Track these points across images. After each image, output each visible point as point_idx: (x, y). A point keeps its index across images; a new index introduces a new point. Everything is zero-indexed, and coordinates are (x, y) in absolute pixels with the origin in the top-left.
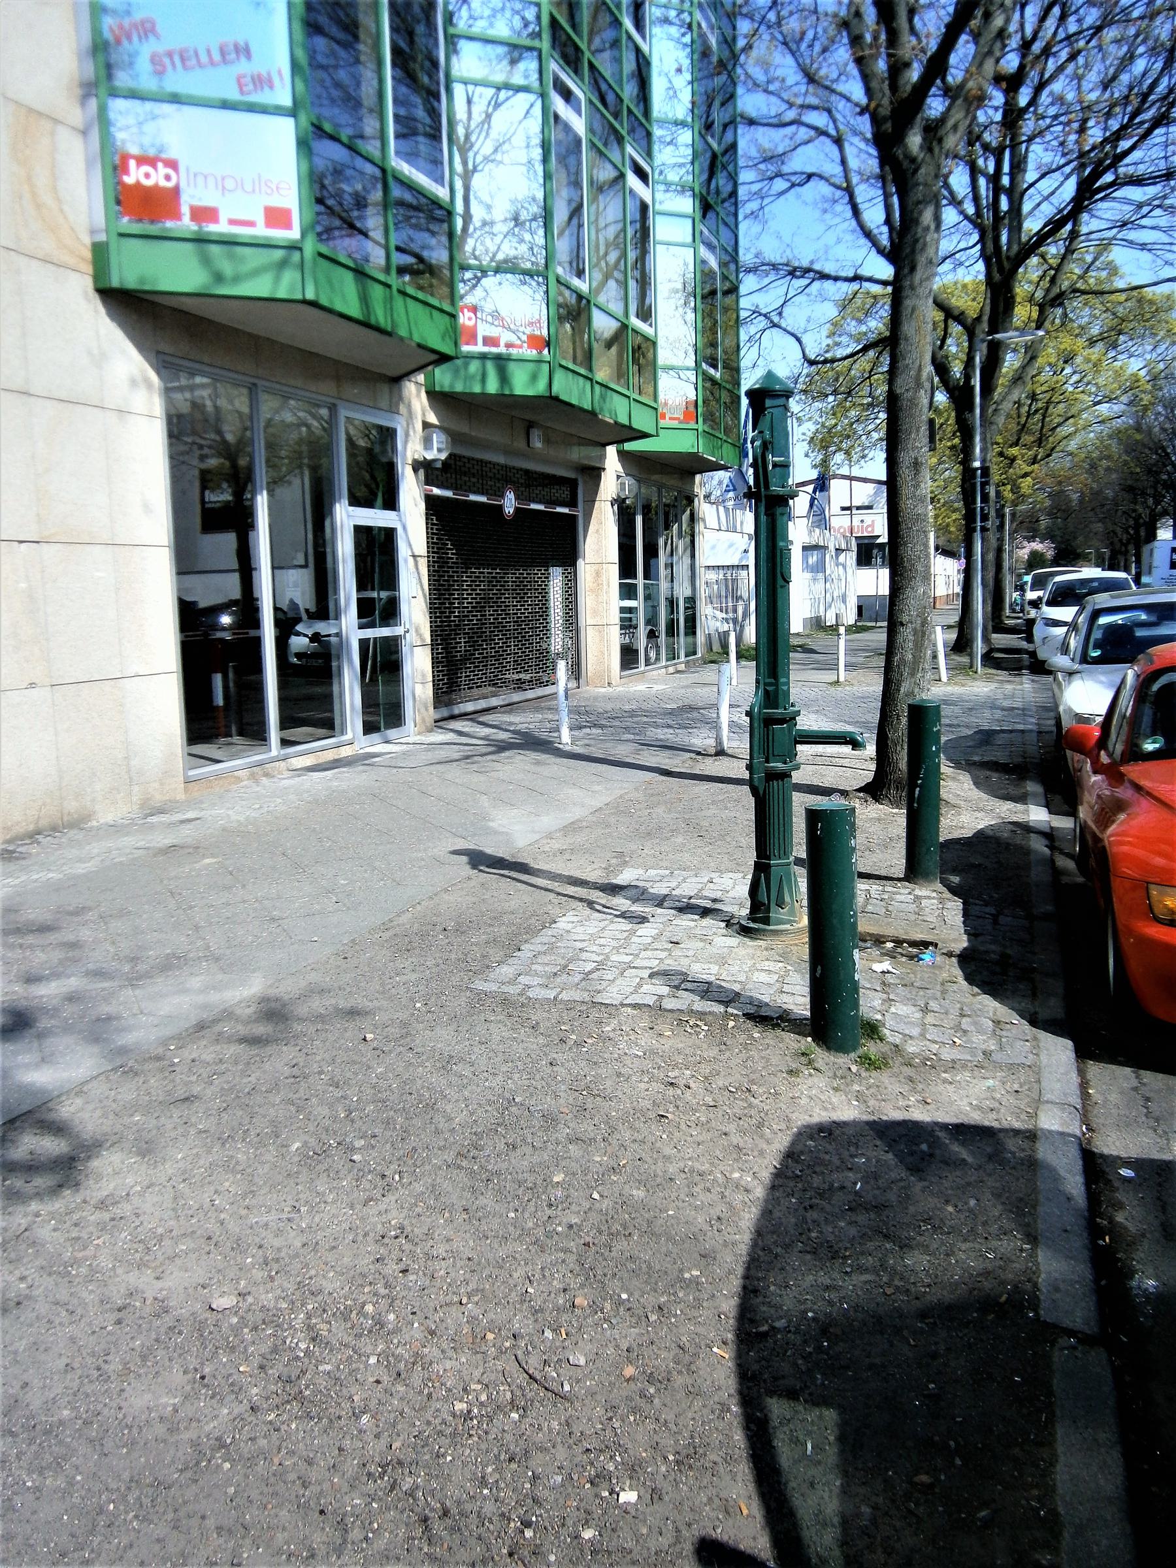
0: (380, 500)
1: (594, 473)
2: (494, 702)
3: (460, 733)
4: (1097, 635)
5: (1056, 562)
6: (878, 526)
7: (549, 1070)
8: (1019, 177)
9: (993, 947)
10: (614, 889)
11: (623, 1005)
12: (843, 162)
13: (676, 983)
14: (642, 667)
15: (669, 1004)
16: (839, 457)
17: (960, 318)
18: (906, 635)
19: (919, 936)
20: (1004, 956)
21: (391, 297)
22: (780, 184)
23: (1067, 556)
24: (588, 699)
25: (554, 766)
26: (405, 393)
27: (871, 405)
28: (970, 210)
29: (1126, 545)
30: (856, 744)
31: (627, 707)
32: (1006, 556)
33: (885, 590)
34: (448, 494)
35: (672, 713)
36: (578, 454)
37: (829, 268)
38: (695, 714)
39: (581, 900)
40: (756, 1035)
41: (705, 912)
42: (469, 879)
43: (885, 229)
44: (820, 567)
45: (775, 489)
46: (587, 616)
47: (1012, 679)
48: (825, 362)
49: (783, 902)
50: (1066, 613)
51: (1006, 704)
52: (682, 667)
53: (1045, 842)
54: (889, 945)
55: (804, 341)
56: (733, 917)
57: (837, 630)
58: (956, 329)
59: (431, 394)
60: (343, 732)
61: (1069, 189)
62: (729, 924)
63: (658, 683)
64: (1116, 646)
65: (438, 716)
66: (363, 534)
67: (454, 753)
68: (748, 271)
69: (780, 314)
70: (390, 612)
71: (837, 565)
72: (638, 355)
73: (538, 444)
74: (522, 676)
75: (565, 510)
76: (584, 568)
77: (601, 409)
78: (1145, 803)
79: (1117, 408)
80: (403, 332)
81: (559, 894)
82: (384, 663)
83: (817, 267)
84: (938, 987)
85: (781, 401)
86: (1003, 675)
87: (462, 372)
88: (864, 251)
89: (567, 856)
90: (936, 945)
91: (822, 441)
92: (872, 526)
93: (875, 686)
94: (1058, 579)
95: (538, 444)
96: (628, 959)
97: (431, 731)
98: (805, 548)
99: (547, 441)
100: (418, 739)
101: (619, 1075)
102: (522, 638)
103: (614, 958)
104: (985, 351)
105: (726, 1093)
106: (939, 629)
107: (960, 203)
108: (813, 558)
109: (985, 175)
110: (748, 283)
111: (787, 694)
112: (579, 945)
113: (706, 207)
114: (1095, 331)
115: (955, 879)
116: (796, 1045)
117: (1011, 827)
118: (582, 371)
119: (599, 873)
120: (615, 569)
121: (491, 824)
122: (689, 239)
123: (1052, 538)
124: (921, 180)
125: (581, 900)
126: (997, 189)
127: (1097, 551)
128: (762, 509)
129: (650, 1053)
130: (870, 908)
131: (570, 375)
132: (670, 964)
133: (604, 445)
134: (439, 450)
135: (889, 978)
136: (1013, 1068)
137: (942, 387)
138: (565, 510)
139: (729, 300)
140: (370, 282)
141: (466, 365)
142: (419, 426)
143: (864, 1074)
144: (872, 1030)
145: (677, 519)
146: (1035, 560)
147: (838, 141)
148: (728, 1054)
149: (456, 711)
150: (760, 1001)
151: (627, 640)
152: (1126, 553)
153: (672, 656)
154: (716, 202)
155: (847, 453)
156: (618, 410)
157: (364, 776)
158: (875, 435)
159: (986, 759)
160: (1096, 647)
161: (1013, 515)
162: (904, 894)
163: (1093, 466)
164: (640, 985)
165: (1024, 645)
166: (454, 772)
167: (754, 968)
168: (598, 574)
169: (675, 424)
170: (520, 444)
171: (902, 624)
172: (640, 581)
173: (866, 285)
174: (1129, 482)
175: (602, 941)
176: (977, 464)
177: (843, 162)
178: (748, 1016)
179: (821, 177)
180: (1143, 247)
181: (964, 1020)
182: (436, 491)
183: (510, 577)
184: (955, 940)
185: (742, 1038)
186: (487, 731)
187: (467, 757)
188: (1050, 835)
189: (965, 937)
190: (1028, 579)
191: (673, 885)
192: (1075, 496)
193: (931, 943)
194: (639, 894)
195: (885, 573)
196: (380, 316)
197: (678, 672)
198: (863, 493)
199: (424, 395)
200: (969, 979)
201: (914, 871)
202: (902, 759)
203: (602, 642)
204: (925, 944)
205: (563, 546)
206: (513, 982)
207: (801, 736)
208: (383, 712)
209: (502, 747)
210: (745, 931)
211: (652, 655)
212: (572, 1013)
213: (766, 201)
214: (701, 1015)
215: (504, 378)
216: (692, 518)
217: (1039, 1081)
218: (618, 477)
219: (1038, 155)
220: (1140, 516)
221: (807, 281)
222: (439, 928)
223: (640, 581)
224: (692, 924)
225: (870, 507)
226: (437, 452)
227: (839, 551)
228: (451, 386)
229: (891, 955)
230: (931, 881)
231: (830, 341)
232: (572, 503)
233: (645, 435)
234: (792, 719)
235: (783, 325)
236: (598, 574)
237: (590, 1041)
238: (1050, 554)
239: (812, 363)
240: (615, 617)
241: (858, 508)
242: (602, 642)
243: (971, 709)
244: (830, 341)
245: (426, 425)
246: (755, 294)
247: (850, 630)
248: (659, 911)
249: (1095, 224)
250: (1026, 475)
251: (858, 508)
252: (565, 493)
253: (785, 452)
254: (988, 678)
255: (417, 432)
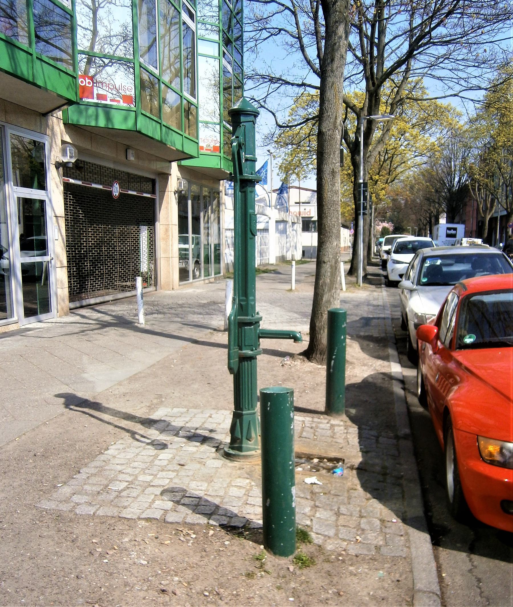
0: (36, 184)
1: (165, 176)
2: (107, 298)
3: (83, 317)
4: (424, 270)
5: (394, 233)
6: (312, 212)
7: (74, 583)
8: (383, 37)
9: (377, 461)
10: (149, 423)
11: (139, 519)
12: (297, 24)
13: (178, 498)
14: (191, 280)
15: (171, 518)
16: (294, 177)
17: (353, 108)
18: (327, 268)
19: (333, 454)
20: (384, 468)
21: (32, 61)
22: (265, 34)
23: (399, 229)
24: (160, 297)
25: (132, 336)
26: (50, 122)
27: (309, 151)
28: (359, 54)
29: (425, 226)
30: (296, 339)
31: (180, 302)
32: (372, 229)
33: (315, 244)
34: (79, 183)
35: (203, 306)
36: (158, 166)
37: (290, 79)
38: (215, 307)
39: (128, 431)
40: (227, 543)
41: (204, 440)
42: (63, 415)
43: (317, 61)
44: (284, 232)
45: (247, 175)
46: (160, 253)
47: (377, 289)
48: (288, 126)
49: (251, 437)
50: (407, 257)
51: (375, 303)
52: (212, 280)
53: (401, 386)
54: (316, 461)
55: (276, 115)
56: (221, 443)
57: (291, 263)
58: (352, 115)
59: (66, 125)
60: (12, 316)
61: (406, 47)
62: (218, 449)
63: (199, 288)
64: (435, 277)
65: (72, 305)
66: (26, 204)
67: (76, 328)
68: (250, 78)
69: (265, 101)
70: (42, 246)
71: (293, 230)
72: (188, 113)
73: (132, 158)
74: (124, 284)
75: (149, 196)
76: (160, 227)
77: (166, 140)
78: (473, 379)
79: (425, 159)
80: (49, 87)
81: (116, 426)
82: (35, 278)
83: (283, 78)
84: (346, 494)
85: (252, 118)
86: (373, 287)
87: (84, 114)
88: (307, 70)
89: (127, 398)
90: (344, 460)
91: (285, 168)
92: (310, 212)
93: (310, 292)
94: (399, 240)
95: (132, 158)
96: (149, 478)
97: (66, 314)
98: (277, 222)
99: (138, 157)
100: (59, 320)
101: (126, 584)
102: (123, 263)
103: (141, 478)
104: (365, 125)
105: (202, 597)
106: (342, 263)
107: (354, 50)
108: (281, 226)
109: (367, 36)
110: (249, 84)
111: (254, 307)
112: (119, 468)
113: (227, 42)
114: (414, 121)
115: (353, 411)
116: (253, 552)
117: (381, 376)
118: (155, 118)
119: (145, 410)
120: (176, 229)
121: (85, 375)
122: (217, 55)
123: (392, 221)
124: (338, 9)
125: (128, 431)
126: (372, 44)
127: (412, 228)
128: (238, 187)
129: (153, 560)
130: (304, 434)
131: (148, 119)
132: (177, 483)
133: (171, 162)
134: (71, 157)
135: (316, 489)
136: (394, 560)
137: (343, 144)
138: (149, 196)
139: (239, 91)
140: (16, 50)
141: (87, 110)
142: (59, 142)
143: (298, 572)
144: (304, 536)
145: (211, 204)
146: (385, 232)
147: (294, 13)
148: (206, 560)
149: (84, 303)
150: (232, 513)
151: (184, 266)
152: (425, 229)
153: (207, 274)
154: (231, 40)
155: (298, 174)
156: (176, 142)
157: (20, 343)
158: (311, 166)
159: (367, 334)
160: (424, 277)
161: (375, 209)
162: (324, 423)
163: (412, 188)
164: (154, 501)
165: (382, 272)
166: (73, 341)
167: (229, 485)
168: (167, 230)
169: (209, 152)
170: (122, 158)
171: (324, 262)
172: (190, 235)
173: (308, 89)
174: (428, 196)
175: (136, 464)
176: (361, 181)
177: (297, 24)
178: (222, 526)
179: (285, 31)
180: (439, 78)
181: (363, 520)
182: (72, 181)
183: (117, 231)
184: (354, 457)
185: (217, 545)
186: (99, 315)
187: (83, 331)
188: (402, 381)
189: (360, 454)
190: (383, 240)
191: (187, 419)
192: (403, 202)
193: (341, 459)
194: (164, 426)
195: (315, 235)
196: (24, 69)
197: (210, 283)
198: (306, 196)
199: (62, 126)
200: (364, 486)
201: (331, 408)
202: (324, 338)
203: (169, 266)
204: (338, 460)
205: (147, 215)
206: (67, 500)
207: (262, 333)
208: (37, 304)
209: (104, 325)
210: (227, 456)
211: (197, 273)
212: (104, 526)
213: (258, 42)
214: (191, 526)
215: (108, 118)
216: (219, 204)
217: (411, 571)
218: (178, 179)
219: (391, 30)
220: (432, 212)
221: (278, 85)
222: (32, 454)
223: (190, 235)
224: (195, 449)
225: (309, 203)
226: (69, 159)
227: (293, 223)
228: (78, 121)
229: (316, 468)
230: (340, 415)
231: (290, 118)
232: (153, 192)
233: (191, 157)
234: (257, 323)
235: (266, 107)
236: (167, 230)
237: (111, 552)
238: (391, 229)
239: (281, 127)
240: (176, 254)
241: (303, 203)
242: (169, 266)
243: (357, 306)
244: (290, 118)
245: (63, 142)
246: (253, 91)
247: (298, 262)
248: (176, 439)
249: (416, 66)
250: (383, 189)
251: (303, 203)
252: (149, 186)
253: (253, 152)
254: (365, 289)
255: (57, 146)
